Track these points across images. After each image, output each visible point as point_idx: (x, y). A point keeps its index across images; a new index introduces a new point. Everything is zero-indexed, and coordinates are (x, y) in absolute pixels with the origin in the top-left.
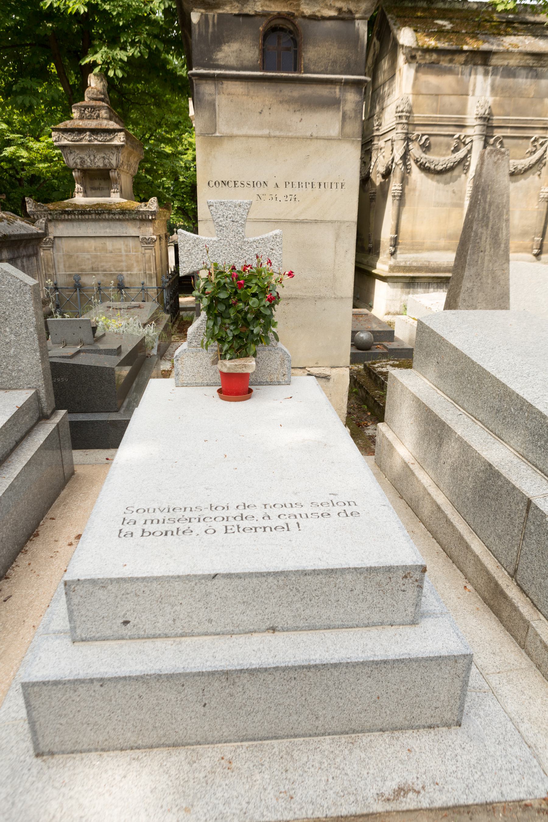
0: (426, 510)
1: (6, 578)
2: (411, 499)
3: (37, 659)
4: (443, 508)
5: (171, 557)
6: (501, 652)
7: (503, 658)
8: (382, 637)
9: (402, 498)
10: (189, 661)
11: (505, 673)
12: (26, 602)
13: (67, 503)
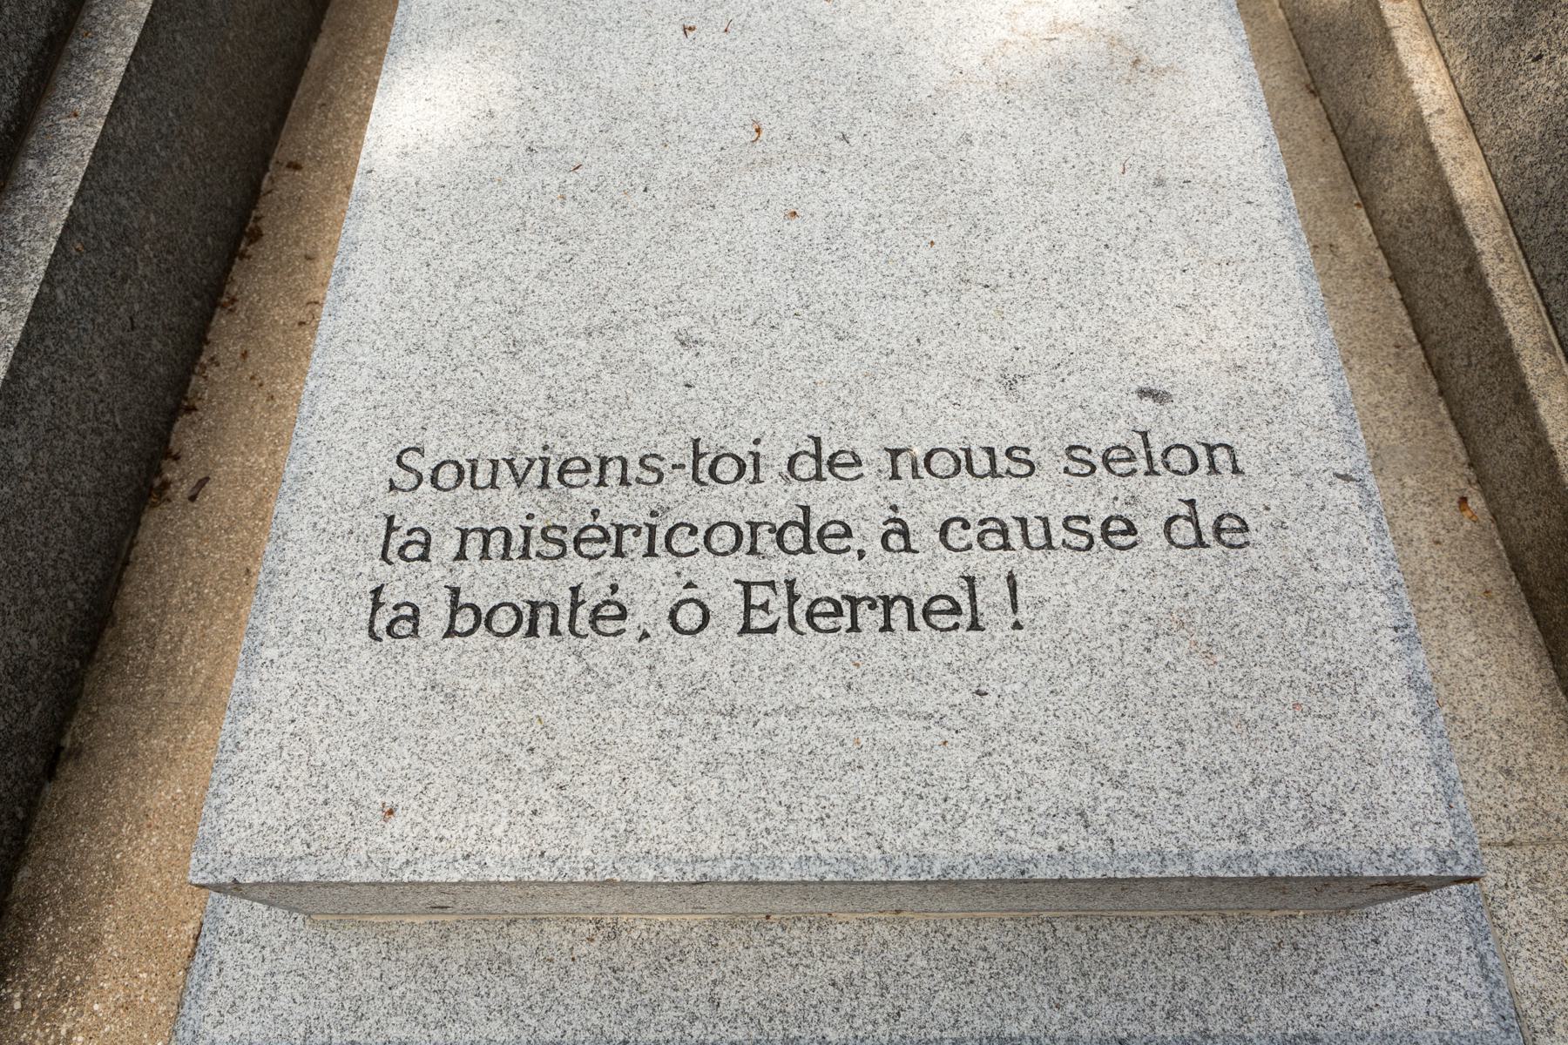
0: (1401, 189)
1: (191, 409)
2: (1351, 119)
3: (214, 969)
4: (1472, 221)
5: (548, 770)
6: (1531, 768)
7: (1531, 795)
8: (1234, 951)
9: (1315, 93)
10: (641, 1013)
11: (1527, 850)
12: (248, 501)
13: (332, 97)
